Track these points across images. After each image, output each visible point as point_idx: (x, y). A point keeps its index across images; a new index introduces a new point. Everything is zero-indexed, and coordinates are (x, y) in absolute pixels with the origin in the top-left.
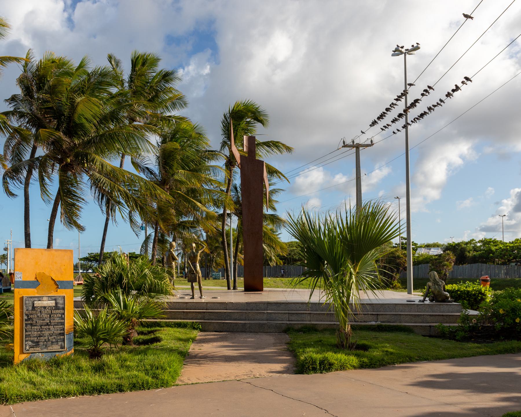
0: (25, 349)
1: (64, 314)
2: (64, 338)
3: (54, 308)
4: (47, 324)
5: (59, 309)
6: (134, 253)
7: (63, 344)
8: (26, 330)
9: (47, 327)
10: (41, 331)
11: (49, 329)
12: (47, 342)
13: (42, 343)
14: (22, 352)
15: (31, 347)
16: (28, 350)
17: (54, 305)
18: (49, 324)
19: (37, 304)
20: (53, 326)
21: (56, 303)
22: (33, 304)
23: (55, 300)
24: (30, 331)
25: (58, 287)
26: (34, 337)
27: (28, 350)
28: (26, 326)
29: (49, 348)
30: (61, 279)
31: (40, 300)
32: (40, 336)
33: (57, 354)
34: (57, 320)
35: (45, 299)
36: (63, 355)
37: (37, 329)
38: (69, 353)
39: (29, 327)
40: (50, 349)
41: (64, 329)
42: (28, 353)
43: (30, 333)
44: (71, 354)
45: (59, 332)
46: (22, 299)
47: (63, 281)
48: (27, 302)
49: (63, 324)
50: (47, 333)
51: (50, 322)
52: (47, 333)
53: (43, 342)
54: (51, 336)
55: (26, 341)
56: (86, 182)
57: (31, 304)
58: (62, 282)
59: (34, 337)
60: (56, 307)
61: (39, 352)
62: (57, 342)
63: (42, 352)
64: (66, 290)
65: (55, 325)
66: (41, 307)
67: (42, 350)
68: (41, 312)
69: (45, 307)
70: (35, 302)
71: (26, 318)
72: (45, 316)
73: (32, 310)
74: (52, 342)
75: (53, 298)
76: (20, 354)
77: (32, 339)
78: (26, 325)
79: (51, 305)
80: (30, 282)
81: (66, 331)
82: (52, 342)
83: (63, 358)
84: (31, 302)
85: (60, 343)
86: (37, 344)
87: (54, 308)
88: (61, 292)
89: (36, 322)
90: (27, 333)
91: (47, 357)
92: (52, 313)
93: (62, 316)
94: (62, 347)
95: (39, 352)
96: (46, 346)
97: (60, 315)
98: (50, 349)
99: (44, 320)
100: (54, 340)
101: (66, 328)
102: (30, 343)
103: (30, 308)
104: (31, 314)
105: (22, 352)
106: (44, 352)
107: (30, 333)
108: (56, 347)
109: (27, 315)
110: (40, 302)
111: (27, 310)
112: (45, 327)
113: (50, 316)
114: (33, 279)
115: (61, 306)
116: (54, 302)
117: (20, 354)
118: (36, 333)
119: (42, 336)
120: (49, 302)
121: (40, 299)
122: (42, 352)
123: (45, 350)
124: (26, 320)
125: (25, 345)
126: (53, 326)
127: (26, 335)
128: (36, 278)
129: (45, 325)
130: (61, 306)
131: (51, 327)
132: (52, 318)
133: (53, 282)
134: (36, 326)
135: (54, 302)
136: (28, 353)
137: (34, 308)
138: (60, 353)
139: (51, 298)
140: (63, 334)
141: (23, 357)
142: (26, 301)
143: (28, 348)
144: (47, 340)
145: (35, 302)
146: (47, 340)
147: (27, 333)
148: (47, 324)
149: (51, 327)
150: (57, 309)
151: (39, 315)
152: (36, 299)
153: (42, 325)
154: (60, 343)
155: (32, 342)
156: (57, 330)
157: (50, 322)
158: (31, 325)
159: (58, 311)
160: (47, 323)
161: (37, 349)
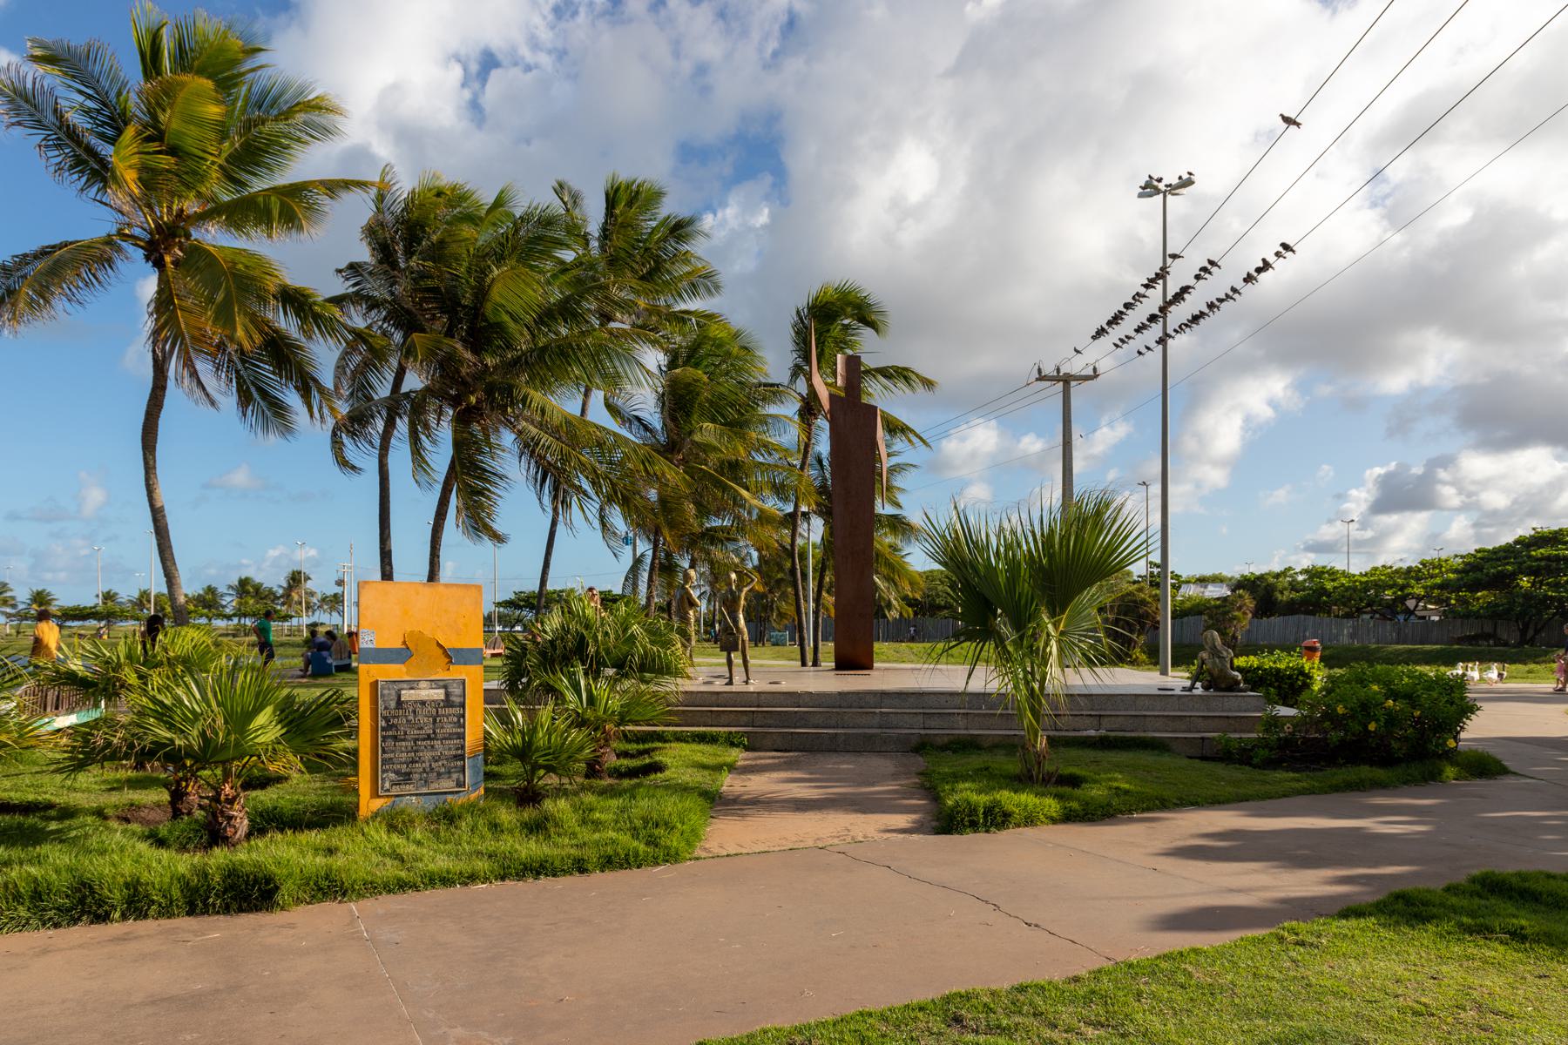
4: (429, 738)
14: (375, 794)
19: (407, 695)
21: (447, 694)
23: (445, 687)
30: (458, 646)
33: (449, 797)
34: (449, 729)
35: (422, 685)
36: (461, 800)
38: (473, 796)
39: (390, 742)
41: (463, 747)
44: (479, 798)
49: (462, 736)
52: (428, 755)
58: (458, 651)
60: (448, 702)
69: (423, 703)
72: (423, 720)
78: (384, 738)
82: (439, 774)
83: (462, 806)
86: (406, 777)
88: (458, 672)
91: (429, 804)
94: (460, 784)
102: (392, 776)
103: (393, 704)
105: (375, 794)
108: (447, 784)
114: (398, 645)
115: (457, 700)
116: (442, 691)
121: (412, 685)
124: (383, 729)
130: (457, 700)
135: (442, 691)
137: (399, 703)
139: (435, 684)
140: (462, 758)
141: (378, 804)
143: (387, 785)
149: (437, 743)
151: (411, 717)
154: (455, 776)
155: (397, 773)
158: (395, 738)
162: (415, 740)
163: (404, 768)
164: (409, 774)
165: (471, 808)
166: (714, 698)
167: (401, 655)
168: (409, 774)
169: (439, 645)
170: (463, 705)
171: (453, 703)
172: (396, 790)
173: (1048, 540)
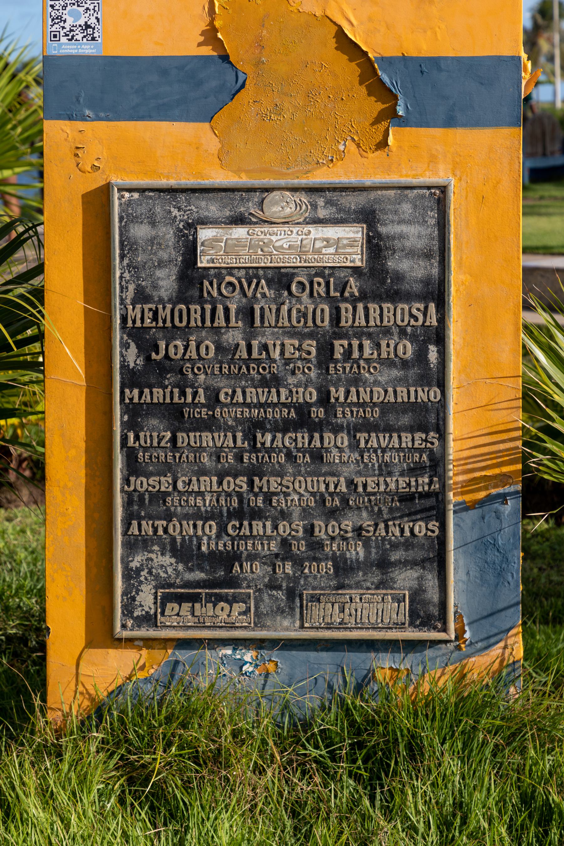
0: (128, 610)
1: (439, 337)
3: (354, 286)
4: (302, 420)
5: (395, 296)
6: (525, 31)
9: (303, 439)
10: (254, 472)
11: (318, 456)
12: (298, 563)
14: (101, 634)
16: (149, 620)
17: (357, 258)
18: (318, 413)
19: (219, 244)
20: (353, 430)
21: (376, 247)
22: (190, 250)
23: (368, 217)
24: (166, 468)
25: (390, 115)
27: (149, 620)
28: (133, 424)
29: (317, 613)
30: (421, 46)
31: (239, 220)
32: (239, 514)
33: (384, 665)
34: (382, 387)
35: (280, 206)
36: (436, 678)
37: (217, 455)
38: (481, 665)
39: (156, 431)
40: (324, 618)
41: (437, 464)
42: (149, 643)
44: (502, 677)
45: (398, 483)
46: (98, 202)
47: (436, 62)
48: (141, 231)
49: (432, 420)
51: (324, 399)
52: (298, 490)
53: (271, 561)
54: (332, 514)
55: (131, 545)
57: (170, 252)
58: (423, 69)
60: (378, 279)
61: (236, 643)
62: (384, 564)
63: (259, 644)
64: (461, 136)
65: (369, 427)
66: (253, 274)
67: (259, 624)
68: (248, 314)
69: (281, 279)
70: (205, 234)
71: (133, 356)
72: (280, 347)
75: (352, 202)
76: (90, 644)
78: (135, 414)
79: (329, 258)
80: (159, 66)
81: (455, 475)
82: (343, 569)
83: (428, 708)
84: (168, 234)
86: (218, 575)
87: (354, 286)
88: (422, 156)
89: (214, 399)
90: (141, 484)
91: (307, 687)
93: (421, 356)
94: (427, 613)
95: (236, 643)
96: (291, 594)
97: (408, 349)
98: (324, 618)
99: (275, 382)
100: (357, 552)
101: (454, 450)
102: (165, 562)
103: (167, 282)
104: (172, 332)
105: (101, 634)
106: (273, 643)
108: (374, 611)
109: (137, 335)
110: (239, 232)
111: (141, 297)
112: (286, 440)
113: (326, 354)
114: (184, 41)
115: (414, 270)
116: (354, 233)
117: (90, 644)
118: (209, 483)
119: (256, 514)
121: (241, 204)
122: (259, 644)
123: (286, 628)
124: (131, 379)
125: (131, 575)
128: (210, 35)
129: (285, 427)
130: (414, 270)
133: (350, 70)
134: (210, 425)
135: (354, 233)
136: (149, 643)
137: (191, 276)
138: (407, 662)
139: (330, 201)
140: (432, 506)
141: (111, 669)
142: (128, 219)
143: (146, 599)
144: (300, 548)
145: (205, 234)
146: (300, 548)
147: (141, 484)
149: (336, 443)
150: (379, 298)
151: (234, 336)
152: (212, 208)
154: (405, 579)
155: (184, 552)
156: (385, 470)
157: (324, 399)
158: (175, 415)
159: (394, 314)
160: (303, 410)
161: (222, 612)
162: (253, 427)
163: (208, 536)
164: (230, 559)
165: (463, 714)
166: (299, 643)
167: (199, 85)
168: (230, 559)
169: (346, 45)
170: (436, 293)
171: (400, 282)
172: (178, 622)
173: (137, 552)
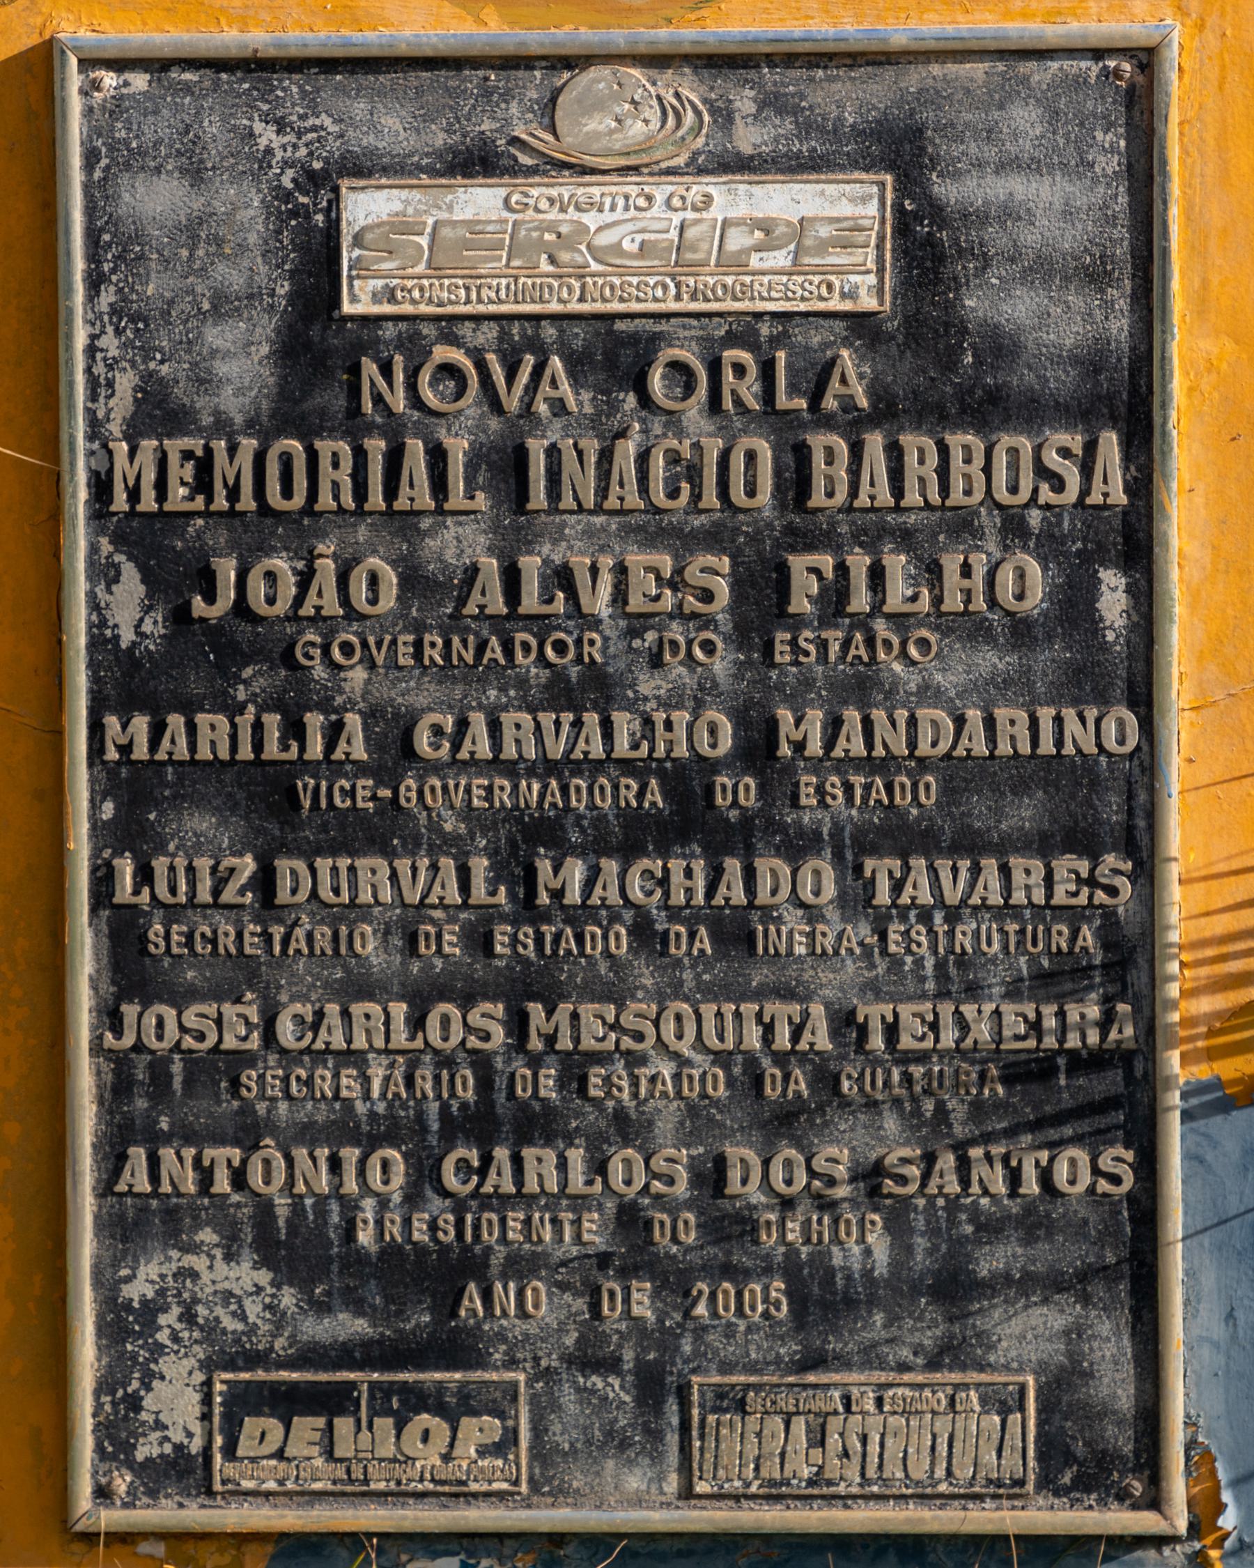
0: (117, 1439)
2: (1145, 1209)
3: (853, 378)
4: (685, 813)
5: (988, 409)
7: (1110, 1346)
8: (124, 935)
9: (687, 875)
10: (527, 988)
11: (736, 933)
12: (675, 1283)
13: (545, 1308)
15: (262, 1391)
16: (186, 1472)
18: (738, 792)
19: (412, 241)
20: (851, 850)
21: (926, 247)
22: (318, 262)
23: (899, 149)
24: (239, 976)
26: (345, 1129)
27: (186, 1472)
28: (130, 832)
29: (735, 1448)
31: (477, 161)
32: (478, 1124)
34: (948, 706)
35: (614, 114)
37: (407, 931)
39: (206, 854)
41: (1127, 959)
43: (237, 1025)
48: (155, 199)
50: (673, 1044)
51: (758, 748)
52: (673, 1044)
53: (588, 1277)
54: (785, 1123)
55: (128, 1228)
56: (467, 505)
57: (252, 264)
59: (345, 1129)
60: (930, 351)
62: (954, 1288)
65: (905, 837)
66: (522, 338)
68: (506, 467)
69: (616, 354)
70: (365, 207)
72: (612, 576)
73: (289, 413)
74: (822, 1304)
75: (847, 100)
77: (290, 1176)
78: (139, 800)
79: (773, 285)
82: (822, 1304)
84: (245, 208)
85: (1026, 1335)
87: (853, 378)
89: (396, 748)
90: (158, 1026)
92: (799, 519)
93: (1075, 603)
96: (652, 1386)
97: (1030, 583)
99: (594, 690)
100: (867, 1246)
101: (1182, 911)
102: (236, 1283)
103: (241, 362)
104: (258, 529)
107: (237, 1025)
109: (153, 544)
110: (480, 201)
111: (158, 412)
113: (762, 594)
116: (853, 203)
118: (380, 1022)
119: (537, 1125)
120: (733, 200)
121: (483, 109)
125: (120, 1324)
126: (851, 850)
127: (117, 1089)
129: (631, 837)
130: (1050, 323)
131: (796, 893)
132: (805, 649)
134: (382, 832)
135: (853, 203)
137: (320, 346)
139: (776, 102)
142: (113, 159)
143: (176, 1403)
144: (678, 1234)
145: (365, 207)
146: (678, 1234)
147: (158, 1026)
148: (685, 813)
150: (935, 415)
151: (462, 542)
152: (389, 124)
153: (538, 833)
154: (1026, 1335)
155: (299, 1249)
156: (958, 978)
157: (758, 748)
158: (270, 803)
159: (986, 466)
160: (688, 782)
161: (425, 1446)
